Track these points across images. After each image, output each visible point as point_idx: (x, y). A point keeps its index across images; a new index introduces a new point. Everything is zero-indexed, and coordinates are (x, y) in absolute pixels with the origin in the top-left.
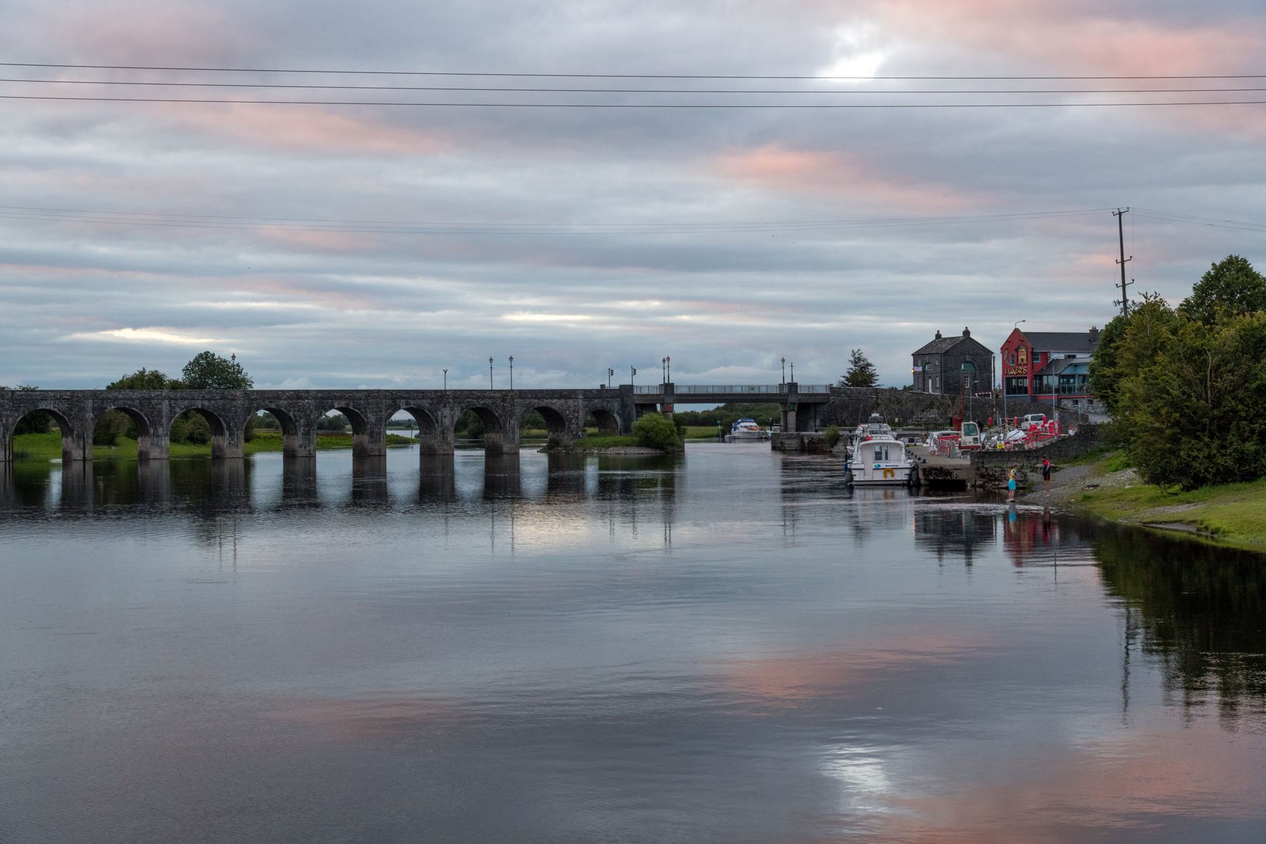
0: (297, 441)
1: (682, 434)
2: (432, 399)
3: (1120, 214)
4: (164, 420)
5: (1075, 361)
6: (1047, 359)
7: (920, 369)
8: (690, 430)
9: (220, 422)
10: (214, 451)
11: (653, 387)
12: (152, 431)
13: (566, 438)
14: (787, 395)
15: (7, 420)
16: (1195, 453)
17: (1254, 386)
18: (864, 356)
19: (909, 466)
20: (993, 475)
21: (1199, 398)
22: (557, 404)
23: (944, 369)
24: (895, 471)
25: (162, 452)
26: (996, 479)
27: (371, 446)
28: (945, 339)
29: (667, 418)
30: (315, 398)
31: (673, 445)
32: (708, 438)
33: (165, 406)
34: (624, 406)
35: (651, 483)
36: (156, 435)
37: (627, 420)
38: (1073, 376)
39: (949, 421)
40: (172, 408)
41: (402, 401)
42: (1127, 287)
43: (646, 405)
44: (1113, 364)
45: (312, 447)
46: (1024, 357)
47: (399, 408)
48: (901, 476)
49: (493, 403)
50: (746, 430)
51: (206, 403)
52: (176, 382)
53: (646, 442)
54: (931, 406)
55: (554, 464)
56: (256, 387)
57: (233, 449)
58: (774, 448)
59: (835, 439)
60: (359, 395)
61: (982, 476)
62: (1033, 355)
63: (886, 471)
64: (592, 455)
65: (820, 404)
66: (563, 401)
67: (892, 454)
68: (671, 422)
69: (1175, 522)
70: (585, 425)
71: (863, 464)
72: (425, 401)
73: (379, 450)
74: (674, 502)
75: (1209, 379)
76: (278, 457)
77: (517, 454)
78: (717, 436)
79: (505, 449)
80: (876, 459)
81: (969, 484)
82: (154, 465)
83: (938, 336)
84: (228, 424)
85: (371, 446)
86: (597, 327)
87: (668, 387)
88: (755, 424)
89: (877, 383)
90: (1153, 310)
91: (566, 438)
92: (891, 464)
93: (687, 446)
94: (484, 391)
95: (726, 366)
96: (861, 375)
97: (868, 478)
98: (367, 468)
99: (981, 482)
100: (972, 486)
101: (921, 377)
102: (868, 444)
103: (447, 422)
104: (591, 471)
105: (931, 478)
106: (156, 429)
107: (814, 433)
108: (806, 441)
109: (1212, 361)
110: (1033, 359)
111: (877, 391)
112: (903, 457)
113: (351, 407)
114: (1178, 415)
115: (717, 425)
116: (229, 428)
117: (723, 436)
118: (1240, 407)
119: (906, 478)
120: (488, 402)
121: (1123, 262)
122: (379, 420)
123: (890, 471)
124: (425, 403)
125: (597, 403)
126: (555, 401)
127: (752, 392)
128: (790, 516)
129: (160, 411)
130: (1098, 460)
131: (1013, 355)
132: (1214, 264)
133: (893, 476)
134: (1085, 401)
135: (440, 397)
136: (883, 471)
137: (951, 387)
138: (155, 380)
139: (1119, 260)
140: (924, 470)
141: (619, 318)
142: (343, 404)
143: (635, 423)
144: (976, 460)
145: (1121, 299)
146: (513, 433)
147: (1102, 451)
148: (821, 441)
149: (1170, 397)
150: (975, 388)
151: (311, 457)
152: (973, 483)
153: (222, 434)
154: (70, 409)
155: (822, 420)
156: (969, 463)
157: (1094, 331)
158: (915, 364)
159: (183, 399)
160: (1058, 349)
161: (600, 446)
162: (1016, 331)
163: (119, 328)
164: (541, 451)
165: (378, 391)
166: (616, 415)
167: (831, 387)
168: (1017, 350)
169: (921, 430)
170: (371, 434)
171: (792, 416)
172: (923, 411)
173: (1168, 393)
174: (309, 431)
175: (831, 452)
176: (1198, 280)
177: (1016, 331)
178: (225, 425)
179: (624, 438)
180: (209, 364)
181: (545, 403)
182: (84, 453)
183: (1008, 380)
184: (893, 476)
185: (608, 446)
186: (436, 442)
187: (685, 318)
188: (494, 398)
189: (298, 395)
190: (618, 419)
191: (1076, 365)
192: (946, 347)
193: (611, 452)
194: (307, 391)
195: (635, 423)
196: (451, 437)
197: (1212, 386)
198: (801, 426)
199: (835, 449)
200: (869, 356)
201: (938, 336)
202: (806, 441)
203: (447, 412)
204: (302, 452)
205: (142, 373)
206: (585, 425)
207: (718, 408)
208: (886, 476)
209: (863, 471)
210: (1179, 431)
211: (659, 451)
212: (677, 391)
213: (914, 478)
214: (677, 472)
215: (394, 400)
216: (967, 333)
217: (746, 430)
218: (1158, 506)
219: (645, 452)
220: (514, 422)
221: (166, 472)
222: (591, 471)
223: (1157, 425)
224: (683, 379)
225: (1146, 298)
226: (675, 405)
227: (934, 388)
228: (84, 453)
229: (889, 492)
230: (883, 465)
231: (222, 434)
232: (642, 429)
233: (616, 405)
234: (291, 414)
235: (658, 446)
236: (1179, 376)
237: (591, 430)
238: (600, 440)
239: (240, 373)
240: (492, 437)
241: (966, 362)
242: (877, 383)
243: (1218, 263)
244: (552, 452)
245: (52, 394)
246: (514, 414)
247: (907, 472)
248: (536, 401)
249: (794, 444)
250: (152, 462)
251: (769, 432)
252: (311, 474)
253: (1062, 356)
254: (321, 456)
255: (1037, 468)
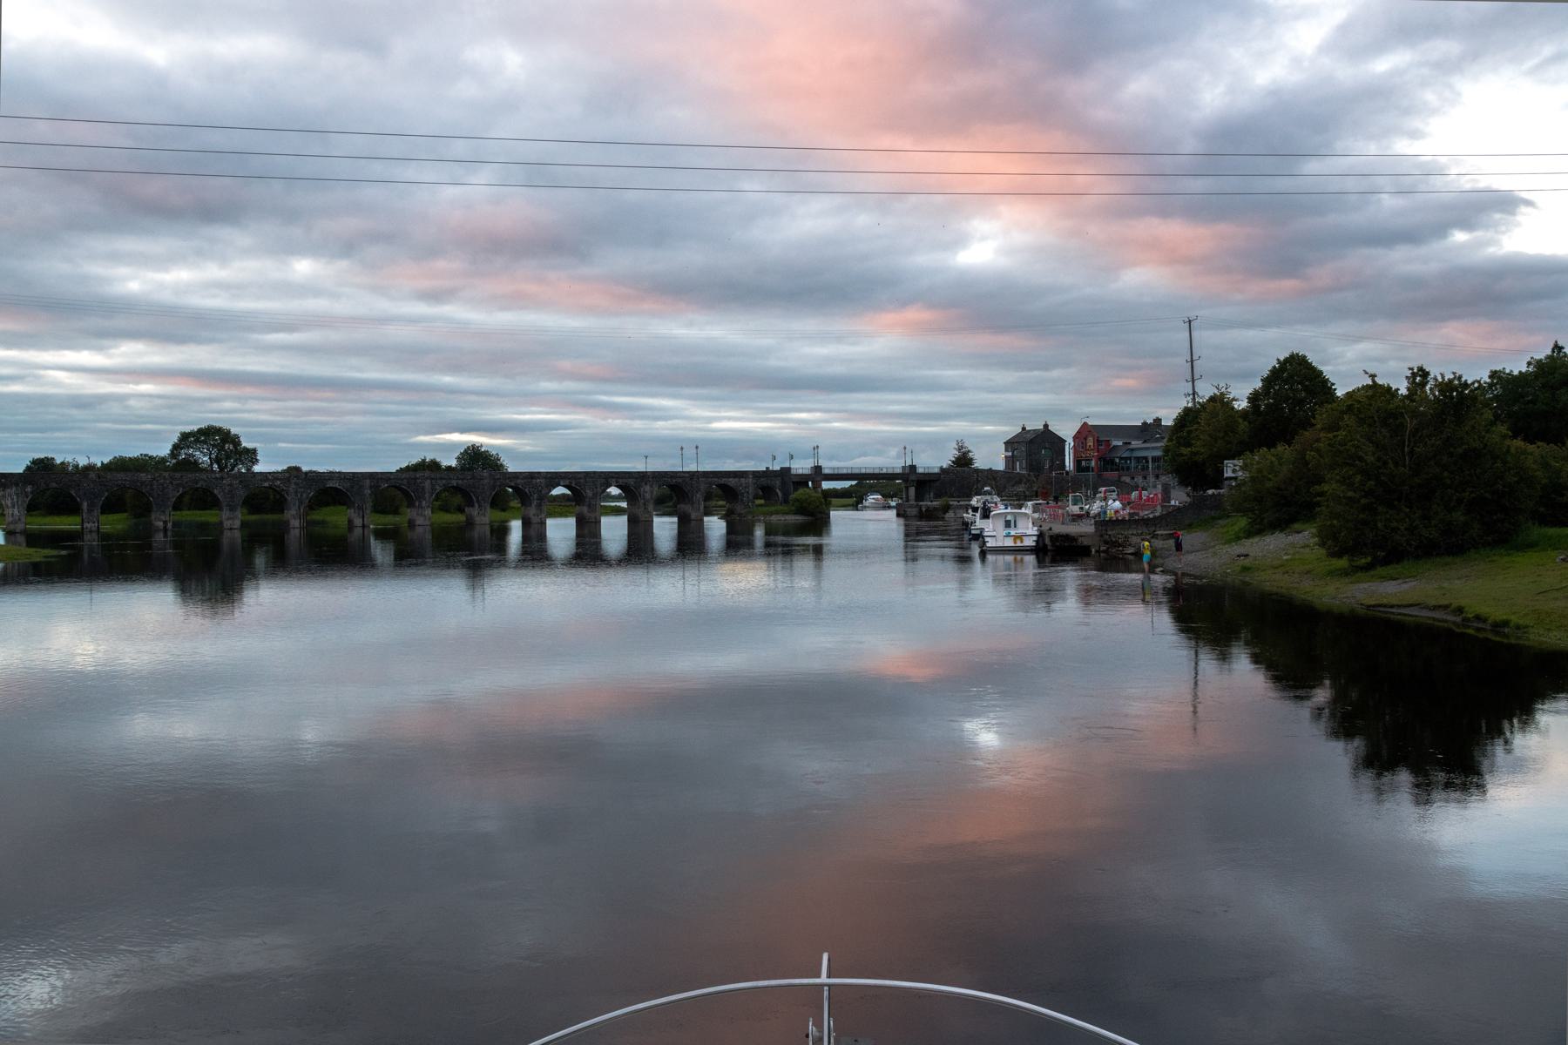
0: (532, 511)
1: (828, 505)
2: (636, 478)
3: (1190, 321)
4: (427, 495)
5: (1131, 447)
6: (1110, 445)
7: (1010, 454)
8: (834, 501)
9: (471, 497)
10: (467, 519)
11: (805, 468)
12: (417, 504)
13: (739, 508)
14: (908, 474)
15: (301, 495)
16: (1394, 524)
17: (1460, 451)
18: (966, 445)
19: (1036, 533)
20: (1116, 542)
21: (1396, 464)
22: (732, 482)
23: (1029, 454)
24: (1024, 538)
25: (425, 520)
26: (1120, 545)
27: (589, 515)
28: (1029, 431)
29: (816, 492)
30: (545, 478)
31: (821, 513)
32: (845, 507)
33: (427, 484)
34: (784, 483)
35: (806, 548)
36: (420, 507)
37: (786, 495)
38: (1130, 458)
39: (1034, 493)
40: (433, 486)
41: (614, 480)
42: (1196, 382)
43: (801, 481)
44: (1188, 445)
45: (543, 516)
46: (1092, 444)
47: (611, 486)
48: (1030, 542)
49: (684, 481)
50: (873, 501)
51: (460, 482)
52: (450, 467)
53: (801, 510)
54: (1020, 482)
55: (731, 530)
56: (510, 470)
57: (484, 517)
58: (898, 515)
59: (946, 508)
60: (579, 476)
61: (1106, 542)
62: (1099, 442)
63: (1016, 538)
64: (759, 521)
65: (933, 481)
66: (737, 480)
67: (1019, 524)
68: (820, 495)
69: (1411, 605)
70: (754, 498)
71: (994, 531)
72: (630, 480)
73: (596, 518)
74: (822, 561)
75: (1407, 443)
76: (572, 521)
77: (702, 520)
78: (853, 505)
79: (693, 517)
80: (1006, 527)
81: (1093, 550)
82: (419, 530)
83: (1024, 429)
84: (477, 498)
85: (589, 515)
86: (776, 431)
87: (818, 469)
88: (880, 497)
89: (976, 465)
90: (1220, 402)
91: (739, 508)
92: (1020, 531)
93: (832, 513)
94: (677, 472)
95: (865, 456)
96: (963, 460)
97: (1000, 544)
98: (586, 531)
99: (1105, 548)
100: (1096, 551)
101: (1010, 461)
102: (292, 442)
103: (648, 496)
104: (759, 533)
105: (1058, 544)
106: (420, 502)
107: (930, 503)
108: (924, 509)
109: (1410, 424)
110: (1099, 445)
111: (977, 471)
112: (1030, 525)
113: (573, 485)
114: (1373, 483)
115: (852, 497)
116: (478, 501)
117: (857, 506)
118: (1446, 474)
119: (1034, 544)
120: (680, 480)
121: (1192, 361)
122: (595, 495)
123: (1020, 537)
124: (631, 482)
125: (763, 481)
126: (731, 479)
127: (881, 472)
128: (911, 557)
129: (423, 488)
130: (1213, 527)
131: (1082, 443)
132: (1278, 360)
133: (1022, 542)
134: (1140, 477)
135: (642, 477)
136: (1012, 538)
137: (1035, 467)
138: (434, 466)
139: (1189, 360)
140: (1051, 537)
141: (792, 425)
142: (567, 482)
143: (793, 496)
144: (1100, 528)
145: (1191, 392)
146: (699, 504)
147: (1214, 518)
148: (935, 509)
149: (1364, 464)
150: (1051, 469)
151: (543, 524)
152: (1097, 548)
153: (473, 506)
154: (352, 487)
155: (935, 494)
156: (1093, 531)
157: (1145, 424)
158: (1006, 450)
159: (441, 479)
160: (1117, 437)
161: (765, 514)
162: (1085, 424)
163: (450, 432)
164: (721, 518)
165: (595, 473)
166: (778, 490)
167: (941, 468)
168: (1086, 439)
169: (1014, 500)
170: (589, 506)
171: (912, 491)
172: (1013, 486)
173: (1361, 459)
174: (540, 503)
175: (943, 518)
176: (1266, 373)
177: (1085, 424)
178: (474, 498)
179: (785, 508)
180: (475, 453)
181: (723, 481)
182: (363, 521)
183: (1078, 462)
184: (1022, 542)
185: (771, 514)
186: (639, 512)
187: (836, 425)
188: (684, 477)
189: (532, 476)
190: (779, 493)
191: (1132, 450)
192: (1029, 437)
193: (774, 518)
194: (539, 473)
195: (793, 496)
196: (651, 507)
197: (1412, 452)
198: (919, 497)
199: (947, 515)
200: (969, 445)
201: (1024, 429)
202: (924, 509)
203: (647, 488)
204: (535, 520)
205: (424, 461)
206: (754, 498)
207: (851, 486)
208: (1015, 543)
209: (994, 539)
210: (1373, 500)
211: (810, 518)
212: (826, 471)
213: (1041, 544)
214: (825, 541)
215: (606, 479)
216: (1046, 426)
217: (873, 501)
218: (1358, 582)
219: (799, 518)
220: (699, 496)
221: (429, 537)
222: (759, 533)
223: (1350, 494)
224: (828, 466)
225: (1218, 389)
226: (823, 482)
227: (1021, 468)
228: (363, 521)
229: (1019, 557)
230: (1013, 533)
231: (473, 506)
232: (798, 500)
233: (778, 483)
234: (527, 490)
235: (811, 514)
236: (1372, 442)
237: (759, 502)
238: (765, 509)
239: (499, 460)
240: (684, 507)
241: (1045, 448)
242: (976, 465)
243: (1282, 359)
244: (729, 519)
245: (337, 475)
246: (699, 490)
247: (1035, 538)
248: (716, 480)
249: (914, 511)
250: (417, 527)
251: (893, 504)
252: (542, 537)
253: (1120, 443)
254: (550, 522)
255: (1157, 535)
